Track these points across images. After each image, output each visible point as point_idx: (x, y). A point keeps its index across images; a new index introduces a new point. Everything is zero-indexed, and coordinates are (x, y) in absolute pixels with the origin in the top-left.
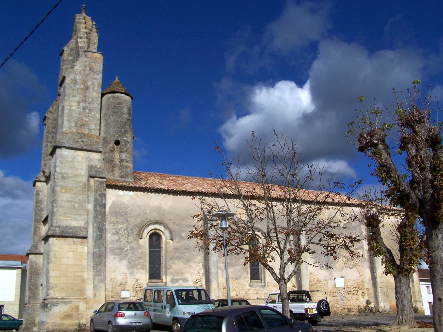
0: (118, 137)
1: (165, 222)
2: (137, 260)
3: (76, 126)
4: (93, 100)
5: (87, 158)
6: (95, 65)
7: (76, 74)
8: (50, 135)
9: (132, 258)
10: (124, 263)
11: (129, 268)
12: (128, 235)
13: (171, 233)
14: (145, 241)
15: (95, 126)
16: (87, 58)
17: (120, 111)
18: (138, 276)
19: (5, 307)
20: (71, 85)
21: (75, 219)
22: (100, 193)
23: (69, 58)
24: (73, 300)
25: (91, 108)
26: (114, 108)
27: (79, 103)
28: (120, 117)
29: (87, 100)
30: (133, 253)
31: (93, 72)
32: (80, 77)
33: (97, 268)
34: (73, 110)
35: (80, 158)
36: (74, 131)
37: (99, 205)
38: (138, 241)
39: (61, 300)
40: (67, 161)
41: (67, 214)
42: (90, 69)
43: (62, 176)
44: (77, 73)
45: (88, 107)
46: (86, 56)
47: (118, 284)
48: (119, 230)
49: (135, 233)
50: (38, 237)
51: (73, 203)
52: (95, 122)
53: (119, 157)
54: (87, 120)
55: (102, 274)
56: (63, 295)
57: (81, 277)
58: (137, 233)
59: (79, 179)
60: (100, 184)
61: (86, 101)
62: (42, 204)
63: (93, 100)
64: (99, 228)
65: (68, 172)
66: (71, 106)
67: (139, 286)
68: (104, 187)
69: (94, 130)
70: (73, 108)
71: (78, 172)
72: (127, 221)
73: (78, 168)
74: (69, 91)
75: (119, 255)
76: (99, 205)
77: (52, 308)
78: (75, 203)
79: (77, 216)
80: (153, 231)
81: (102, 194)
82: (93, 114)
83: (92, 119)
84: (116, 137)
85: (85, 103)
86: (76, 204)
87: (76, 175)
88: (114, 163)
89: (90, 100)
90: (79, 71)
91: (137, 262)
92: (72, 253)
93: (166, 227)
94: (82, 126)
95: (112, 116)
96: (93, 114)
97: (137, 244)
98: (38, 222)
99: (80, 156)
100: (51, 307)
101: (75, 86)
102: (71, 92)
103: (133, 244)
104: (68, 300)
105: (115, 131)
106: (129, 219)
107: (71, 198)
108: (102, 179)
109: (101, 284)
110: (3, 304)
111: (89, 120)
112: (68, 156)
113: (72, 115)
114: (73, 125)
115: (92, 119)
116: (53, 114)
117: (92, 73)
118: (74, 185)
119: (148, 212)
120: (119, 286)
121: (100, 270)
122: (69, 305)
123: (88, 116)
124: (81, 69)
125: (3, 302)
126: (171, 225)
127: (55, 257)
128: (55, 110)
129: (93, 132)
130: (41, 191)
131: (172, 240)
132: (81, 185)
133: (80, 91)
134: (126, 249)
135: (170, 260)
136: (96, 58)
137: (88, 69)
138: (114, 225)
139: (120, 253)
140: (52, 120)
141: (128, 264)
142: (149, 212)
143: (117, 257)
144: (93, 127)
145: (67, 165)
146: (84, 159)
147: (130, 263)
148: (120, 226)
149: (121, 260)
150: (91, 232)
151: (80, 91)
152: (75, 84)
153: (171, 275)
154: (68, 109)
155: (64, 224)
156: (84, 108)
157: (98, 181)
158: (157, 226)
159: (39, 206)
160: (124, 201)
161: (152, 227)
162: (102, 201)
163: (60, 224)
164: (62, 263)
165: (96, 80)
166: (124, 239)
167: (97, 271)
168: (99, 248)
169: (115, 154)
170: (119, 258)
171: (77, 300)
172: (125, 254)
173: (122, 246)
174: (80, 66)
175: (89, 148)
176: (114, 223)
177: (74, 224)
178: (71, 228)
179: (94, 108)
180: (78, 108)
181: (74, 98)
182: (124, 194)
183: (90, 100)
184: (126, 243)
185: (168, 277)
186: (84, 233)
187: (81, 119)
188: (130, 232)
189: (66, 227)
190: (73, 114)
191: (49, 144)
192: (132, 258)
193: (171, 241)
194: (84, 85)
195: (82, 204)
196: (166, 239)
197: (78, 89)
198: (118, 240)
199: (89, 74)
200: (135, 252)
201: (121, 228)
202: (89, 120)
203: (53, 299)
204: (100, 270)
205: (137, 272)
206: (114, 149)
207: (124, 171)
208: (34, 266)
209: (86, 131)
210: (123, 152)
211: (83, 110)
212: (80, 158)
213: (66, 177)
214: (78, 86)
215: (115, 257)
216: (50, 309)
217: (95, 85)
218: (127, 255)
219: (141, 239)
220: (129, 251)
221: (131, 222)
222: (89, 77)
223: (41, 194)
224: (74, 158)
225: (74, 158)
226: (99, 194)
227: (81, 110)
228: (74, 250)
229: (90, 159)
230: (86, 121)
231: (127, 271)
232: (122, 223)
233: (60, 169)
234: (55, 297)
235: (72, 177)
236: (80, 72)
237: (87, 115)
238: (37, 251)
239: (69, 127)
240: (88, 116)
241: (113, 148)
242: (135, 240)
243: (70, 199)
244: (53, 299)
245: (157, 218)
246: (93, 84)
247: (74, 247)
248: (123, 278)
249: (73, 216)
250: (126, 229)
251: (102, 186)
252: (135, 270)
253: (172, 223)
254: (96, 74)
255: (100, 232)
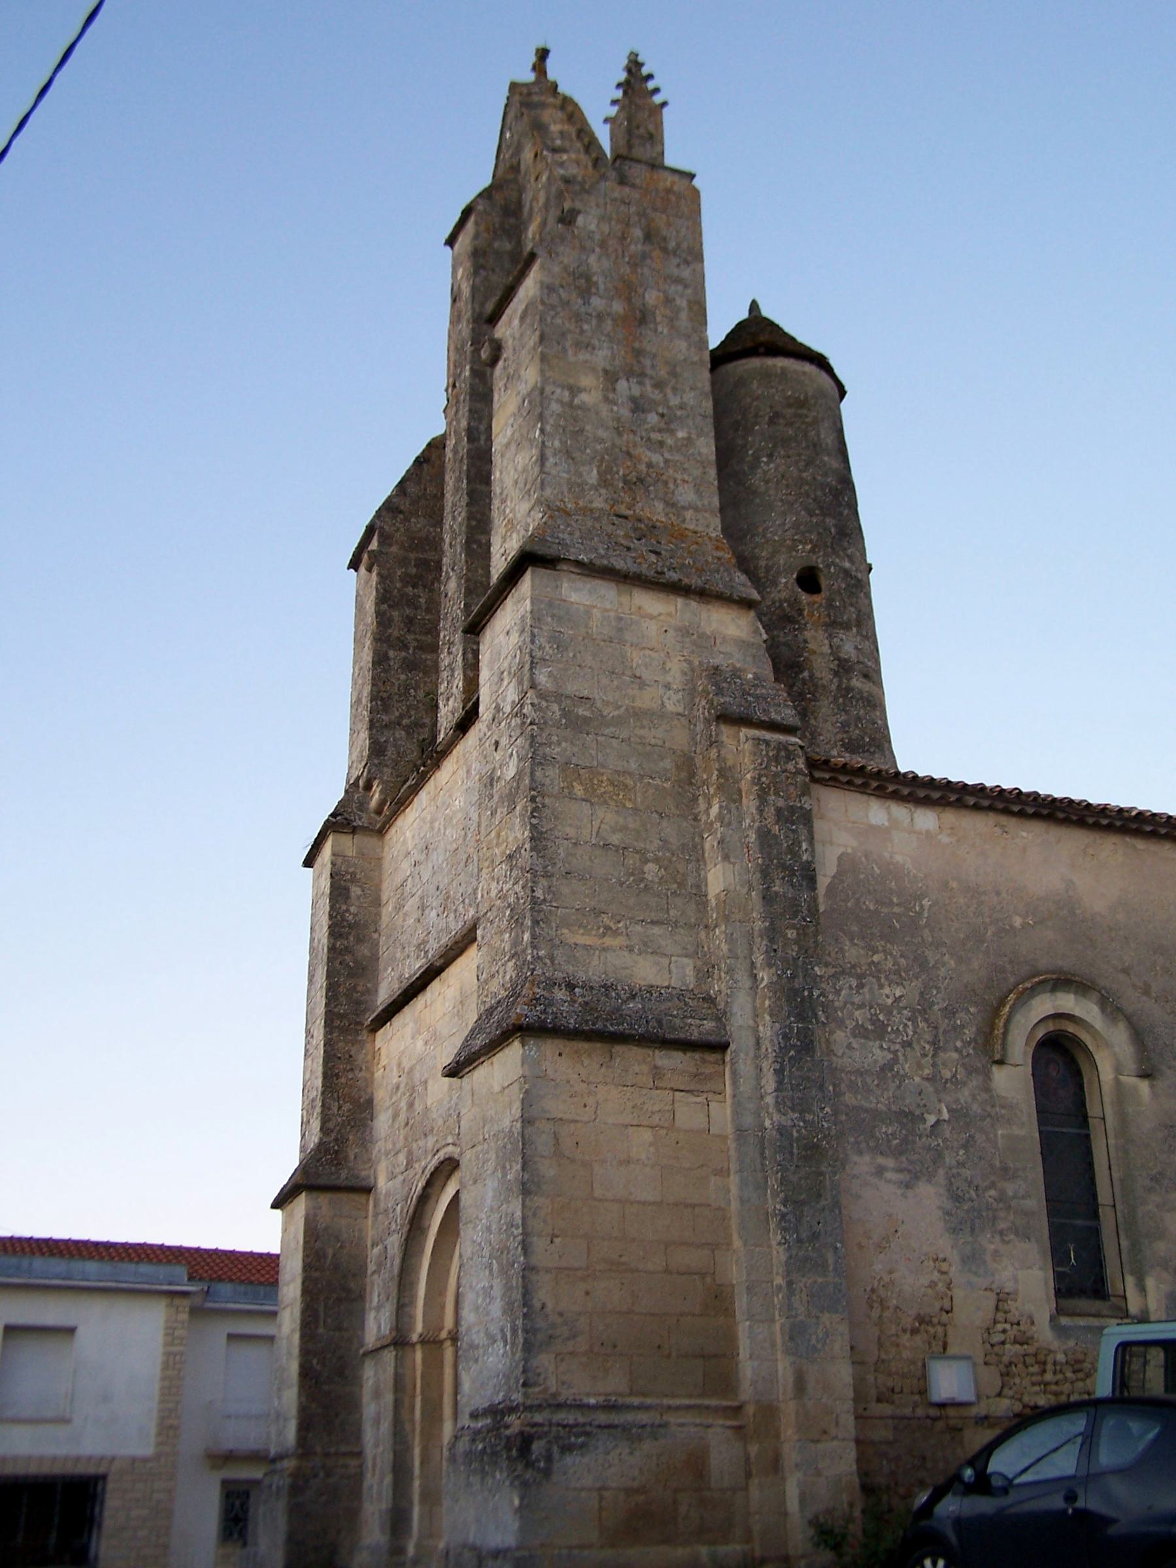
0: (812, 550)
1: (1102, 982)
2: (993, 1185)
3: (604, 481)
4: (674, 374)
5: (685, 632)
6: (669, 225)
7: (583, 248)
8: (395, 614)
9: (967, 1173)
10: (930, 1197)
11: (954, 1231)
12: (934, 1043)
13: (1138, 1036)
14: (1013, 1082)
15: (698, 492)
16: (627, 190)
17: (805, 435)
18: (1005, 1274)
19: (110, 1486)
20: (563, 294)
21: (648, 948)
22: (781, 803)
23: (496, 245)
24: (671, 1418)
25: (669, 408)
26: (772, 422)
27: (611, 378)
28: (808, 464)
29: (649, 372)
30: (965, 1146)
31: (664, 250)
32: (606, 264)
33: (799, 1220)
34: (582, 407)
35: (652, 629)
36: (598, 503)
37: (784, 867)
38: (988, 1076)
39: (602, 1418)
40: (588, 636)
41: (606, 919)
42: (648, 237)
43: (565, 713)
44: (588, 244)
45: (657, 404)
46: (623, 181)
47: (908, 1321)
48: (889, 1012)
49: (969, 1033)
50: (347, 1107)
51: (632, 861)
52: (697, 472)
53: (826, 649)
54: (656, 458)
55: (830, 1258)
56: (614, 1383)
57: (703, 1275)
58: (979, 1031)
59: (654, 735)
60: (776, 759)
61: (643, 374)
62: (360, 940)
63: (674, 374)
64: (796, 992)
65: (597, 695)
66: (574, 390)
67: (1012, 1332)
68: (799, 772)
69: (696, 509)
70: (584, 397)
71: (646, 699)
72: (923, 964)
73: (647, 675)
74: (558, 321)
75: (898, 1153)
76: (784, 867)
77: (556, 1466)
78: (647, 861)
79: (657, 930)
80: (1051, 1027)
81: (792, 810)
82: (681, 434)
83: (677, 457)
84: (803, 554)
85: (640, 383)
86: (651, 867)
87: (638, 714)
88: (806, 674)
89: (663, 373)
90: (597, 237)
91: (992, 1193)
92: (647, 1135)
93: (1111, 1007)
94: (636, 484)
95: (770, 456)
96: (681, 434)
97: (985, 1096)
98: (344, 1031)
99: (652, 617)
100: (549, 1459)
101: (586, 302)
102: (570, 326)
103: (964, 1095)
104: (644, 1417)
105: (796, 526)
106: (932, 957)
107: (624, 829)
108: (782, 738)
109: (825, 1318)
110: (102, 1470)
111: (666, 461)
112: (588, 613)
113: (582, 430)
114: (593, 476)
115: (677, 457)
116: (407, 520)
117: (656, 253)
118: (633, 766)
119: (1018, 921)
120: (914, 1331)
121: (815, 1236)
122: (647, 1446)
123: (661, 444)
124: (606, 228)
125: (102, 1459)
126: (1132, 1000)
127: (558, 1154)
128: (413, 503)
129: (691, 521)
130: (354, 879)
131: (1145, 1075)
132: (667, 763)
133: (608, 325)
134: (931, 1119)
135: (1150, 1190)
136: (669, 191)
137: (638, 233)
138: (861, 986)
139: (905, 1141)
140: (402, 547)
141: (948, 1205)
142: (1025, 926)
143: (890, 1163)
144: (686, 495)
145: (589, 661)
146: (671, 633)
147: (957, 1198)
148: (889, 993)
149: (912, 1178)
150: (751, 1019)
151: (608, 325)
152: (586, 292)
153: (1165, 1275)
154: (560, 401)
155: (593, 970)
156: (638, 406)
157: (767, 743)
158: (1067, 1002)
159: (347, 950)
160: (898, 858)
161: (1044, 1005)
162: (793, 851)
163: (570, 969)
164: (598, 1193)
165: (680, 288)
166: (920, 1066)
167: (799, 1241)
168: (802, 1106)
169: (807, 635)
170: (900, 1170)
171: (689, 1418)
172: (929, 1149)
173: (910, 1102)
174: (602, 218)
175: (695, 581)
176: (860, 977)
177: (645, 972)
178: (633, 997)
179: (682, 407)
180: (607, 400)
181: (583, 356)
182: (894, 824)
183: (663, 373)
184: (929, 1088)
185: (1150, 1283)
186: (709, 1025)
187: (628, 454)
188: (944, 1025)
189: (607, 987)
190: (588, 428)
191: (391, 654)
192: (967, 1173)
193: (1144, 1086)
194: (629, 300)
195: (681, 867)
196: (1118, 1070)
197: (600, 317)
198: (887, 1067)
199: (644, 256)
200: (980, 1138)
201: (897, 1000)
202: (666, 461)
203: (559, 1406)
204: (815, 1236)
205: (996, 1254)
206: (800, 612)
207: (859, 719)
208: (330, 1252)
209: (657, 512)
210: (847, 627)
211: (633, 411)
212: (652, 629)
213: (586, 720)
214: (597, 302)
215: (881, 1160)
216: (547, 1473)
217: (679, 310)
218: (938, 1156)
219: (1001, 1062)
220: (946, 1130)
221: (942, 972)
222: (646, 271)
223: (355, 891)
224: (621, 626)
225: (621, 626)
226: (779, 811)
227: (625, 413)
228: (655, 1120)
229: (702, 636)
230: (650, 465)
231: (945, 1245)
232: (898, 976)
233: (550, 674)
234: (566, 1395)
235: (619, 721)
236: (603, 244)
237: (656, 436)
238: (343, 1177)
239: (571, 485)
240: (661, 444)
241: (794, 602)
242: (971, 1071)
243: (615, 839)
244: (559, 1406)
245: (1067, 962)
246: (668, 301)
247: (658, 1101)
248: (932, 1285)
249: (639, 928)
250: (922, 1010)
251: (790, 766)
252: (989, 1243)
253: (1134, 986)
254: (675, 261)
255: (801, 1017)
